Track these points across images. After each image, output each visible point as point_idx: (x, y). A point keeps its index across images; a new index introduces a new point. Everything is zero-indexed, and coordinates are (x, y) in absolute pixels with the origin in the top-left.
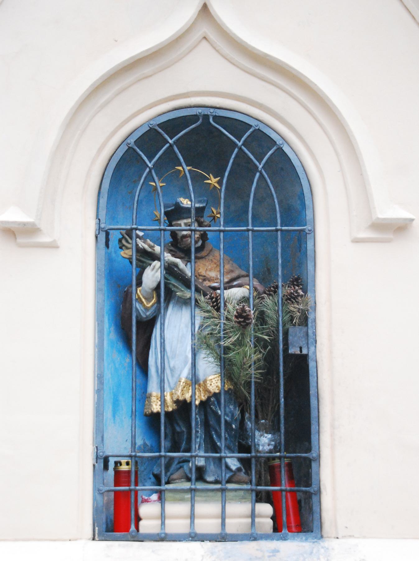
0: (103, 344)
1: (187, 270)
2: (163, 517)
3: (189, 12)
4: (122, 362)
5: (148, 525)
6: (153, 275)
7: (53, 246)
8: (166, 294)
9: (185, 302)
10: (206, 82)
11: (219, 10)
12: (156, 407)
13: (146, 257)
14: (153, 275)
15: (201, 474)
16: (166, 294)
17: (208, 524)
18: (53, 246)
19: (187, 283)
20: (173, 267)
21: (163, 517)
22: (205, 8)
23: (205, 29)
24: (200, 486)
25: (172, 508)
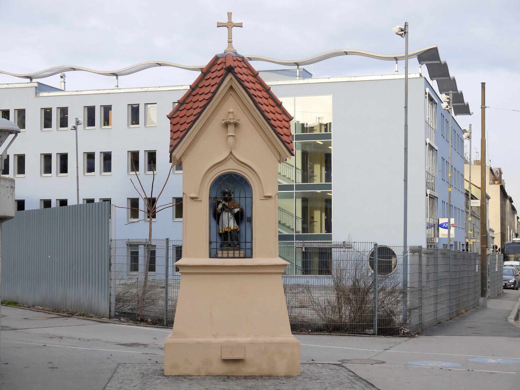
0: (407, 269)
1: (227, 204)
2: (222, 254)
3: (228, 153)
4: (214, 222)
5: (220, 255)
6: (220, 206)
7: (201, 201)
8: (223, 209)
9: (226, 211)
10: (231, 167)
11: (233, 153)
12: (221, 232)
13: (219, 202)
14: (220, 206)
15: (230, 245)
16: (223, 209)
17: (237, 255)
18: (201, 201)
19: (227, 207)
20: (376, 265)
21: (222, 254)
22: (231, 153)
23: (231, 156)
24: (230, 248)
25: (236, 252)
